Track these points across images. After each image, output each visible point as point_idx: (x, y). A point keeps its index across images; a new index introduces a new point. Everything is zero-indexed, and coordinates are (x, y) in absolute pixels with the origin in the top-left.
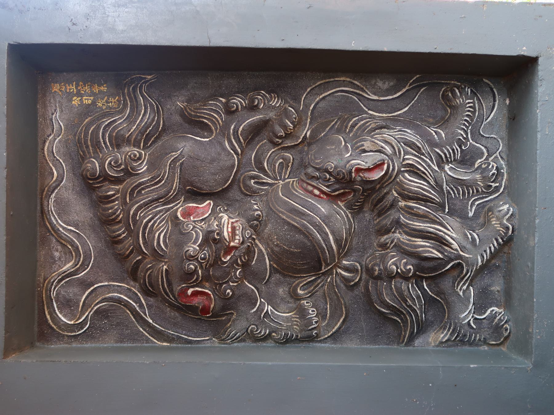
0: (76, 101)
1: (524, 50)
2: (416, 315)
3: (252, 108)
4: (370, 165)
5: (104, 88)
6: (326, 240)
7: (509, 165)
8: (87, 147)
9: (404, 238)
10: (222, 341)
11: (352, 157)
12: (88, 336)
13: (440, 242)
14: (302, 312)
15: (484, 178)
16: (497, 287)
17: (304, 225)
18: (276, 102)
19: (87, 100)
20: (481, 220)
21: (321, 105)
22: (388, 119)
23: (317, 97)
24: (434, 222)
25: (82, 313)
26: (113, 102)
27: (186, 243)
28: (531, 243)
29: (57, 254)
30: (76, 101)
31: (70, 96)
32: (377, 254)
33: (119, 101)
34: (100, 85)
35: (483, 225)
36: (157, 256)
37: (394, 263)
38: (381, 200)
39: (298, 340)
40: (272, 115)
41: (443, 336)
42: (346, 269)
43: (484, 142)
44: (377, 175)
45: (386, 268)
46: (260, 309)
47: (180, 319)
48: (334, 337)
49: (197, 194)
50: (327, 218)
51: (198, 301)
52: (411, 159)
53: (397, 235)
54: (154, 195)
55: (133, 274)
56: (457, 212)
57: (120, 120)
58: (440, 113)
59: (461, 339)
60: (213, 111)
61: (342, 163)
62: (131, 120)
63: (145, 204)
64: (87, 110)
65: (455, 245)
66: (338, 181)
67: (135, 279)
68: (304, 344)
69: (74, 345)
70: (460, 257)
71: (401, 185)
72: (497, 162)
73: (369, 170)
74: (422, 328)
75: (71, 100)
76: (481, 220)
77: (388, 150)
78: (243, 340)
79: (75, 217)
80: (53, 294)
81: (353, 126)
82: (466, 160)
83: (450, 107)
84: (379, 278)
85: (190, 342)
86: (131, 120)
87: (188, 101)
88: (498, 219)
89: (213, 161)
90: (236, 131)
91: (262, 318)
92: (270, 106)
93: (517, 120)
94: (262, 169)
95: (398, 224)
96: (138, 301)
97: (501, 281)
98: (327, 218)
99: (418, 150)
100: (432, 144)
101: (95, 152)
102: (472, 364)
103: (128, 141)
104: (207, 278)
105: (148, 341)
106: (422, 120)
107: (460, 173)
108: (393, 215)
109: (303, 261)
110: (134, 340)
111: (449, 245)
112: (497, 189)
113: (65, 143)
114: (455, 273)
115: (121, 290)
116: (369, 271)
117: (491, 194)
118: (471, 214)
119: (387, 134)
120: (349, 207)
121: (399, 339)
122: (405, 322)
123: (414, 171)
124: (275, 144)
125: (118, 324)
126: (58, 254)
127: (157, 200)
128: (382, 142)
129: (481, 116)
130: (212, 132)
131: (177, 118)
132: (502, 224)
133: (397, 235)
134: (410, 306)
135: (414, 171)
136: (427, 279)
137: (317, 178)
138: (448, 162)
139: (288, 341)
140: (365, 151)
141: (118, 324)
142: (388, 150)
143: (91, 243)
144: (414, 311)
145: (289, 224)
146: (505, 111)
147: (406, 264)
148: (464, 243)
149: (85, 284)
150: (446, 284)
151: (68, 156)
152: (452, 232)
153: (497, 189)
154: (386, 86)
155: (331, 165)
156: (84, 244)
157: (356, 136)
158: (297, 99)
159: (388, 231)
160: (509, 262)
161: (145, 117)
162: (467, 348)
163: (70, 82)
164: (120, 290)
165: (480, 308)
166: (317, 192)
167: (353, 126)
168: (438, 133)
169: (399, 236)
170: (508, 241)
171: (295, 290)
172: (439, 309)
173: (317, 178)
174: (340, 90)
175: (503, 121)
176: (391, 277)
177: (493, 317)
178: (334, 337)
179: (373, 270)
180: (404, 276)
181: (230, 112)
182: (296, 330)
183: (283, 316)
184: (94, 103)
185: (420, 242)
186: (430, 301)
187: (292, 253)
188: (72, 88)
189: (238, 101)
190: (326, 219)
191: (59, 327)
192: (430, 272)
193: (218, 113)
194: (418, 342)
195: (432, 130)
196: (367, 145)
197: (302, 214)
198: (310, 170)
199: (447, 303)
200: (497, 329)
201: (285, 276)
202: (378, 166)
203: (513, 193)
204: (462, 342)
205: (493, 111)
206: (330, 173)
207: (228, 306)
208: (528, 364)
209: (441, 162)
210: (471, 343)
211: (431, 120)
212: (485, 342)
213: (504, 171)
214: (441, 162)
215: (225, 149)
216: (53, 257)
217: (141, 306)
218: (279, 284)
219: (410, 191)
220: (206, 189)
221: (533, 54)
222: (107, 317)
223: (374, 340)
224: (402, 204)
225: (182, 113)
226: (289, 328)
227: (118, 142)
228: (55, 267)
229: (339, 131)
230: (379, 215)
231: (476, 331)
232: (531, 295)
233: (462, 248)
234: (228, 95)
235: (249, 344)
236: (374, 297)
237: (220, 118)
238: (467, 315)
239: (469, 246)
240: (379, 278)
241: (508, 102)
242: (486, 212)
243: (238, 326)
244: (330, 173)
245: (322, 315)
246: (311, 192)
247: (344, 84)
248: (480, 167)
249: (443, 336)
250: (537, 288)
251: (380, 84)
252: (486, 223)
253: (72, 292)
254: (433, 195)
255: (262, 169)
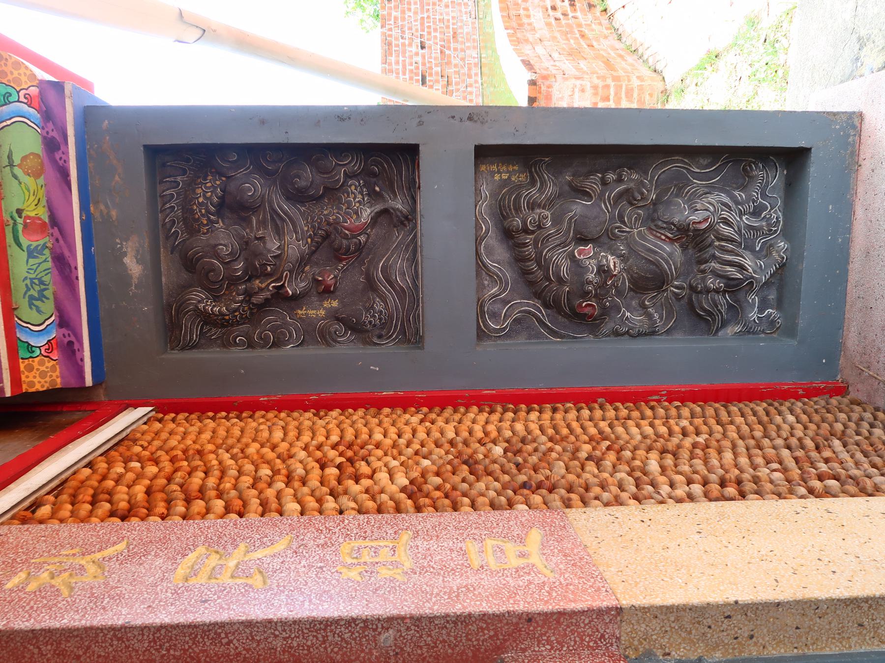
0: (497, 177)
1: (803, 144)
2: (722, 316)
3: (620, 180)
4: (700, 219)
5: (516, 168)
6: (670, 269)
7: (784, 215)
8: (510, 210)
9: (717, 266)
10: (596, 336)
11: (690, 214)
12: (507, 336)
13: (741, 268)
14: (650, 316)
15: (769, 225)
16: (772, 296)
17: (657, 260)
18: (635, 176)
19: (505, 176)
20: (764, 253)
21: (662, 176)
22: (706, 186)
23: (659, 172)
24: (737, 255)
25: (504, 321)
26: (522, 177)
27: (586, 273)
28: (800, 268)
29: (486, 282)
30: (497, 177)
31: (493, 174)
32: (699, 276)
33: (526, 176)
34: (513, 165)
35: (766, 256)
36: (561, 281)
37: (711, 282)
38: (702, 241)
39: (645, 334)
40: (632, 185)
41: (737, 329)
42: (677, 287)
43: (768, 199)
44: (704, 226)
45: (705, 286)
46: (624, 315)
47: (568, 323)
48: (668, 332)
49: (582, 240)
50: (669, 253)
51: (588, 311)
52: (725, 214)
53: (713, 264)
54: (558, 242)
55: (538, 295)
56: (750, 248)
57: (534, 191)
58: (741, 181)
59: (749, 331)
60: (593, 183)
61: (683, 218)
62: (541, 190)
63: (553, 248)
64: (504, 183)
65: (751, 270)
66: (678, 230)
67: (539, 298)
68: (648, 337)
69: (498, 342)
70: (753, 277)
71: (717, 231)
72: (776, 214)
73: (700, 222)
74: (724, 324)
75: (493, 177)
76: (764, 253)
77: (712, 208)
78: (609, 336)
79: (497, 257)
80: (486, 309)
81: (687, 193)
82: (756, 213)
83: (748, 177)
84: (700, 292)
85: (576, 338)
86: (541, 190)
87: (573, 175)
88: (777, 252)
89: (596, 217)
90: (609, 197)
91: (624, 320)
92: (632, 177)
93: (793, 186)
94: (624, 223)
95: (714, 257)
96: (541, 312)
97: (775, 292)
98: (669, 253)
99: (729, 207)
100: (737, 203)
101: (517, 212)
102: (762, 344)
103: (539, 206)
104: (596, 296)
105: (547, 338)
106: (729, 186)
107: (753, 222)
108: (711, 251)
109: (649, 282)
110: (538, 338)
111: (747, 270)
112: (776, 231)
113: (490, 206)
114: (747, 288)
115: (531, 305)
116: (692, 289)
117: (771, 235)
118: (758, 249)
119: (711, 198)
120: (681, 246)
121: (709, 332)
122: (714, 320)
123: (726, 222)
124: (631, 204)
125: (527, 328)
126: (366, 214)
127: (559, 245)
128: (707, 205)
129: (767, 182)
130: (592, 198)
131: (567, 188)
132: (779, 256)
133: (713, 264)
134: (719, 310)
135: (726, 222)
136: (728, 292)
137: (664, 228)
138: (745, 214)
139: (640, 335)
140: (697, 210)
141: (527, 328)
142: (712, 208)
143: (509, 275)
144: (721, 313)
145: (646, 259)
146: (783, 179)
147: (719, 283)
148: (756, 268)
149: (505, 302)
150: (741, 295)
151: (492, 215)
152: (748, 262)
153: (776, 231)
154: (705, 163)
155: (676, 220)
156: (504, 275)
157: (689, 200)
158: (646, 173)
159: (706, 262)
160: (781, 280)
161: (551, 189)
162: (751, 336)
163: (493, 164)
164: (528, 305)
165: (761, 311)
166: (663, 237)
167: (687, 193)
168: (739, 195)
169: (714, 265)
170: (782, 266)
171: (643, 302)
172: (736, 311)
173: (664, 228)
174: (675, 166)
175: (782, 185)
176: (708, 291)
177: (770, 315)
178: (668, 332)
179: (697, 287)
180: (717, 291)
181: (604, 183)
182: (645, 328)
183: (636, 319)
184: (509, 178)
185: (729, 268)
186: (730, 306)
187: (647, 278)
188: (495, 168)
189: (611, 176)
190: (670, 255)
191: (489, 331)
192: (733, 287)
193: (595, 183)
194: (720, 334)
195: (736, 193)
196: (699, 206)
197: (655, 252)
198: (660, 223)
199: (741, 307)
200: (772, 323)
201: (636, 293)
202: (706, 220)
203: (786, 234)
204: (749, 332)
205: (775, 179)
206: (675, 225)
207: (605, 312)
208: (795, 343)
209: (741, 214)
210: (754, 333)
211: (734, 185)
212: (763, 332)
213: (781, 219)
214: (741, 214)
215: (602, 209)
216: (483, 285)
217: (543, 315)
218: (632, 298)
219: (724, 235)
220: (590, 237)
221: (808, 146)
222: (520, 323)
223: (692, 333)
224: (717, 243)
225: (570, 184)
226: (640, 327)
227: (532, 206)
228: (485, 291)
229: (677, 196)
230: (700, 251)
231: (758, 325)
232: (799, 300)
233: (755, 272)
234: (604, 171)
235: (612, 338)
236: (696, 305)
237: (598, 188)
238: (753, 315)
239: (758, 270)
240: (700, 292)
241: (785, 172)
242: (768, 248)
243: (607, 328)
244: (675, 225)
245: (661, 318)
246: (660, 238)
247: (678, 161)
248: (765, 217)
249: (737, 329)
250: (803, 295)
251: (701, 161)
252: (768, 254)
253: (497, 306)
254: (737, 237)
255: (624, 223)
